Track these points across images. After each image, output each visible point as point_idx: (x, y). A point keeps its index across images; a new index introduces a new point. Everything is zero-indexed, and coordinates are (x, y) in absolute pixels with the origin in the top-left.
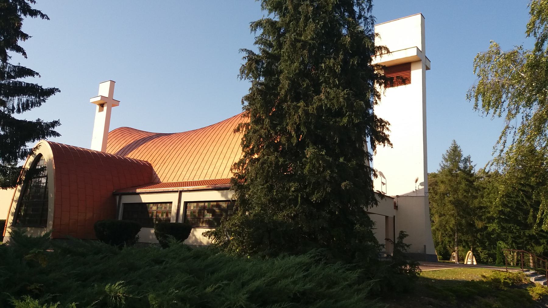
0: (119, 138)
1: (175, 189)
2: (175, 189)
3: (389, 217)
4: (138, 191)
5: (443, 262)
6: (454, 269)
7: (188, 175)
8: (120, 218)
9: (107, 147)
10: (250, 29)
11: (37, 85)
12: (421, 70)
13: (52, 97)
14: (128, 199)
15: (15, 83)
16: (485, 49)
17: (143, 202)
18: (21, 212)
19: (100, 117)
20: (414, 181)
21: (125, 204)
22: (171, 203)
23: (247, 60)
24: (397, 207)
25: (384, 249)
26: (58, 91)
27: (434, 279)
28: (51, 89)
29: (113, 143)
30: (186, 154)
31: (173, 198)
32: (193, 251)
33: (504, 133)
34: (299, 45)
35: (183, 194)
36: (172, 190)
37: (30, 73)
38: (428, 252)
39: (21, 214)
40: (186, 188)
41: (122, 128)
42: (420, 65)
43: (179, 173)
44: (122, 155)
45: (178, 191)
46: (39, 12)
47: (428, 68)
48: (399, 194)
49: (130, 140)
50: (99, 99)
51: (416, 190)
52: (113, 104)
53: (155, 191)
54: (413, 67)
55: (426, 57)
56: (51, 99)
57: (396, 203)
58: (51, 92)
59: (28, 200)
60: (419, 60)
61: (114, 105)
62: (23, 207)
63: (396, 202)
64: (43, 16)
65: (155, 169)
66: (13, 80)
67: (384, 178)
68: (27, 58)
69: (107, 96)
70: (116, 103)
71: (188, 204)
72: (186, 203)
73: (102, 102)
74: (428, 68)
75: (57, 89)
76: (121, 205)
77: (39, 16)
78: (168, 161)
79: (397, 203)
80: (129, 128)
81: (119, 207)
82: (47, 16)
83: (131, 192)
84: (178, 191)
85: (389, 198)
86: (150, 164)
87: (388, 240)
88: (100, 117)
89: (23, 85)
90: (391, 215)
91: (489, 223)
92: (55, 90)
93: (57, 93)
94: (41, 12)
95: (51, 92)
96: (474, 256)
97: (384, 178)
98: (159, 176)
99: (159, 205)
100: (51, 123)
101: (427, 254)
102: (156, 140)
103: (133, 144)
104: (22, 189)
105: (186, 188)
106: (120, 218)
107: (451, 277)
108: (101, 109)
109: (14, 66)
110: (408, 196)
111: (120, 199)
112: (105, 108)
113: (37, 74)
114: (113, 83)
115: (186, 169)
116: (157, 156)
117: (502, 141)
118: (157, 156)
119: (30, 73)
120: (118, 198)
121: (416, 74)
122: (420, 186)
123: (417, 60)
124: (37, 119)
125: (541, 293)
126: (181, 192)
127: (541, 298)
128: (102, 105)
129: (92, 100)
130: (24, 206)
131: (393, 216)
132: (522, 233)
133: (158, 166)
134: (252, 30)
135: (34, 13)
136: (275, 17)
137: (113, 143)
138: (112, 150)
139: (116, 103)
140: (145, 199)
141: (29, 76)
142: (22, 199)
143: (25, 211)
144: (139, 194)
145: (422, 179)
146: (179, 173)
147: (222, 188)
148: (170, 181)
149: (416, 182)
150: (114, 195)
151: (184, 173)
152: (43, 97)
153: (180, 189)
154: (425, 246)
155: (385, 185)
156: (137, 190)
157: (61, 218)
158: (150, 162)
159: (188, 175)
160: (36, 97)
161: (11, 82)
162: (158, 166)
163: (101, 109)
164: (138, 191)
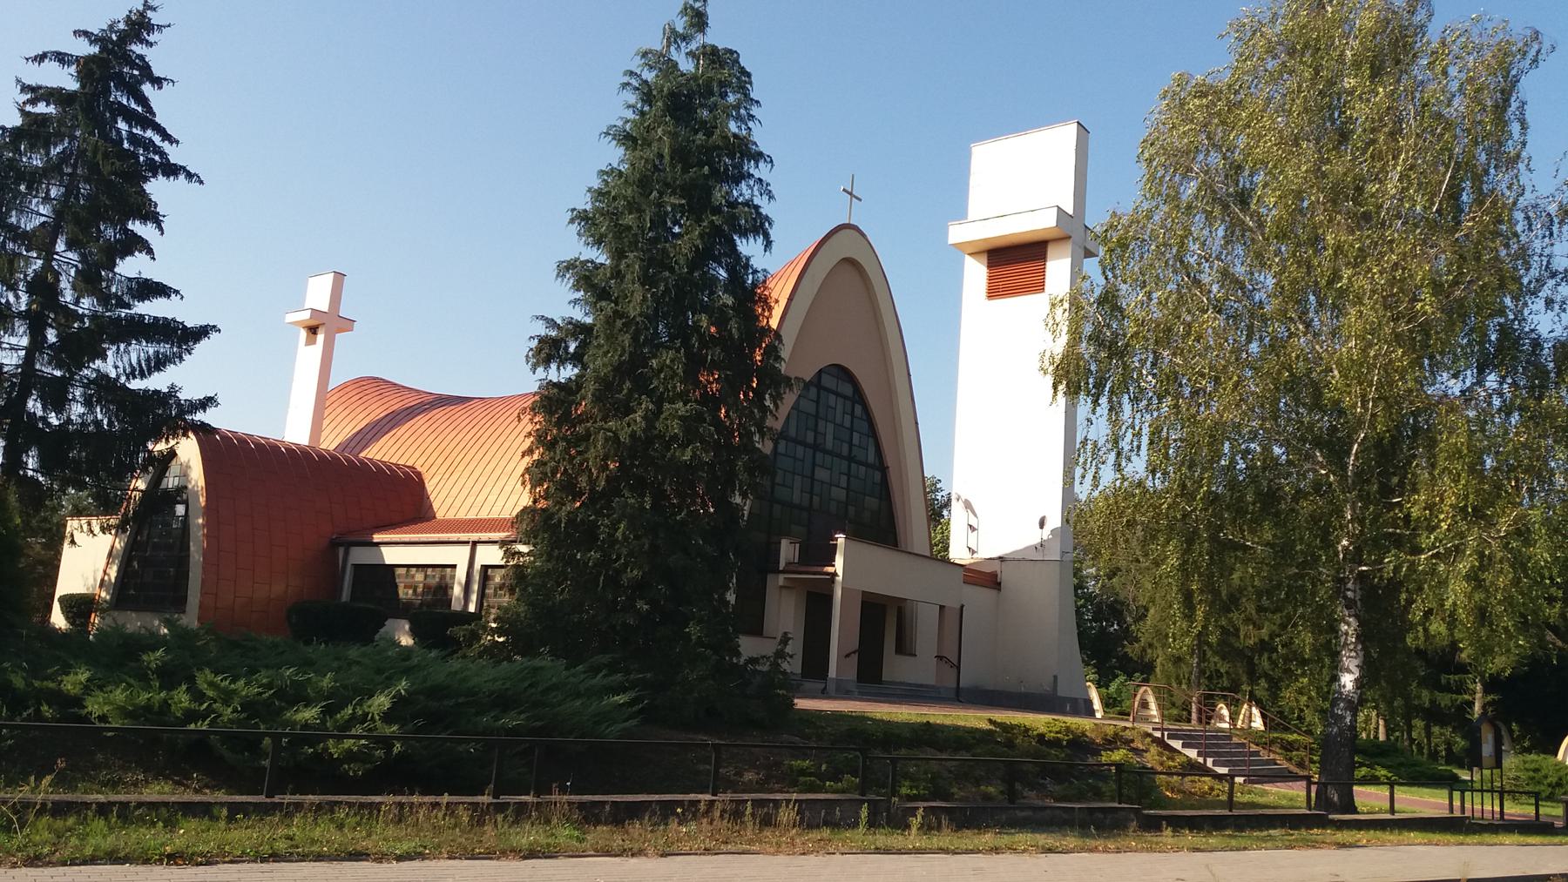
0: (353, 407)
1: (463, 537)
2: (463, 537)
4: (377, 538)
7: (500, 503)
8: (346, 596)
9: (324, 427)
10: (555, 273)
11: (174, 320)
12: (1068, 261)
13: (204, 342)
14: (360, 556)
15: (132, 318)
17: (387, 562)
19: (309, 356)
21: (356, 567)
22: (454, 566)
23: (536, 341)
28: (201, 327)
29: (339, 418)
30: (499, 455)
31: (457, 556)
32: (1132, 829)
34: (619, 323)
35: (480, 548)
36: (455, 539)
37: (162, 290)
40: (485, 536)
42: (1068, 248)
43: (481, 498)
45: (468, 542)
46: (184, 168)
49: (377, 411)
50: (306, 315)
53: (422, 540)
54: (1051, 251)
56: (202, 347)
58: (202, 332)
63: (999, 573)
65: (429, 487)
66: (127, 311)
67: (975, 515)
68: (154, 259)
69: (326, 310)
70: (347, 324)
71: (490, 570)
72: (485, 568)
75: (214, 327)
76: (349, 569)
77: (182, 177)
78: (461, 468)
80: (378, 378)
84: (468, 542)
86: (419, 474)
88: (309, 356)
89: (146, 321)
90: (952, 603)
93: (214, 335)
94: (188, 168)
95: (202, 332)
97: (975, 515)
98: (435, 506)
99: (430, 570)
100: (200, 400)
102: (437, 413)
103: (385, 421)
105: (485, 536)
106: (346, 596)
108: (311, 341)
109: (130, 279)
110: (1024, 560)
111: (347, 554)
112: (320, 337)
113: (177, 292)
114: (339, 277)
115: (496, 490)
116: (435, 454)
118: (435, 454)
119: (162, 290)
120: (341, 551)
124: (169, 384)
126: (475, 544)
128: (313, 330)
129: (292, 317)
133: (435, 480)
134: (558, 276)
135: (172, 170)
136: (601, 257)
137: (339, 418)
138: (330, 442)
139: (347, 324)
140: (391, 556)
141: (160, 296)
144: (378, 544)
145: (1055, 521)
146: (481, 498)
148: (461, 515)
150: (334, 544)
151: (492, 498)
152: (186, 343)
153: (474, 536)
154: (1055, 677)
156: (374, 536)
157: (216, 594)
158: (419, 469)
159: (500, 503)
160: (172, 345)
161: (123, 315)
162: (435, 480)
163: (311, 341)
164: (377, 538)
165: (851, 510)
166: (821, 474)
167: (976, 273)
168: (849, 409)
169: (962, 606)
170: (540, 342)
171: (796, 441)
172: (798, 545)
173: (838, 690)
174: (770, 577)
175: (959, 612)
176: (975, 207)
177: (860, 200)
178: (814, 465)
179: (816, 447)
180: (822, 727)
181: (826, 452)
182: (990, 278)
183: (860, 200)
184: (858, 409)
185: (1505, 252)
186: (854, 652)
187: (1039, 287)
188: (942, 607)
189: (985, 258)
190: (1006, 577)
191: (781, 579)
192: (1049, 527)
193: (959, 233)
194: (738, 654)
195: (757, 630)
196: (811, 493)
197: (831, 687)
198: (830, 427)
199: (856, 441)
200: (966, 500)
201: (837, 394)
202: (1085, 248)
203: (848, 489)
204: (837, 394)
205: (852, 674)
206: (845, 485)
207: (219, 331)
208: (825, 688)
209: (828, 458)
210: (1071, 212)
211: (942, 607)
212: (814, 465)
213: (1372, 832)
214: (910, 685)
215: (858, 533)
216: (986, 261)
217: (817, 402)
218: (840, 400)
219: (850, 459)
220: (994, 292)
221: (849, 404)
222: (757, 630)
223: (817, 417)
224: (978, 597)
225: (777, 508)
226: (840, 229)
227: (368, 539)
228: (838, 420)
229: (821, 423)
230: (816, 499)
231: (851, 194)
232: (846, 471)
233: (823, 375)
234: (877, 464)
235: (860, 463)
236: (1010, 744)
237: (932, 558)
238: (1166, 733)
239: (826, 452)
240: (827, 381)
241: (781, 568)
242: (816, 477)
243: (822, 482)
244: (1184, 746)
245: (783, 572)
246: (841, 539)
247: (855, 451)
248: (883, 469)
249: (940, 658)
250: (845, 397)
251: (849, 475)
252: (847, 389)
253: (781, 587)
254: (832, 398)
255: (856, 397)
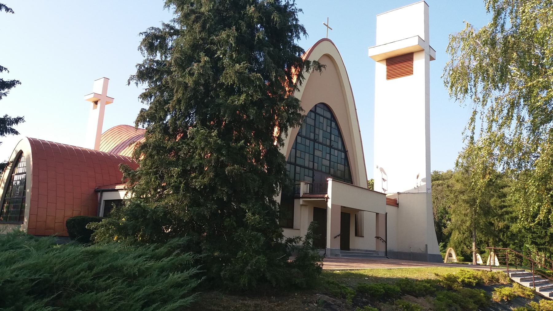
3: (379, 214)
4: (117, 187)
5: (463, 263)
6: (426, 269)
12: (424, 60)
13: (13, 89)
14: (108, 196)
16: (460, 28)
18: (3, 209)
20: (416, 177)
24: (398, 204)
25: (301, 241)
26: (19, 84)
27: (368, 277)
33: (473, 120)
34: (193, 17)
38: (430, 252)
39: (4, 211)
41: (121, 126)
44: (115, 153)
46: (4, 6)
47: (433, 58)
48: (400, 191)
51: (417, 186)
52: (106, 102)
55: (430, 46)
57: (397, 200)
59: (10, 197)
60: (422, 49)
61: (107, 103)
62: (5, 204)
63: (397, 199)
64: (7, 9)
70: (110, 100)
73: (96, 100)
74: (432, 59)
75: (18, 81)
79: (398, 201)
81: (100, 204)
82: (11, 10)
83: (110, 188)
85: (380, 194)
87: (378, 238)
90: (382, 212)
91: (513, 222)
92: (16, 82)
93: (17, 86)
94: (6, 6)
95: (11, 84)
96: (496, 256)
100: (15, 119)
101: (429, 254)
104: (5, 186)
107: (388, 275)
108: (95, 108)
110: (409, 193)
111: (101, 195)
113: (6, 69)
114: (107, 79)
117: (472, 127)
120: (99, 194)
121: (419, 63)
122: (422, 182)
123: (417, 51)
125: (508, 294)
127: (509, 299)
128: (96, 103)
130: (6, 203)
131: (385, 214)
132: (544, 232)
138: (106, 148)
139: (110, 100)
142: (5, 196)
143: (8, 208)
144: (117, 190)
145: (423, 175)
147: (18, 163)
149: (417, 178)
150: (96, 192)
154: (426, 245)
155: (386, 182)
156: (116, 186)
163: (95, 108)
165: (332, 170)
166: (317, 153)
167: (382, 68)
168: (329, 124)
169: (386, 214)
170: (146, 36)
171: (306, 138)
172: (308, 185)
173: (331, 254)
174: (296, 201)
175: (385, 216)
176: (380, 38)
177: (331, 29)
178: (314, 149)
179: (315, 141)
180: (344, 288)
181: (319, 143)
182: (388, 71)
183: (331, 29)
184: (333, 124)
185: (533, 101)
186: (338, 236)
187: (410, 72)
188: (377, 214)
189: (385, 62)
190: (401, 201)
191: (301, 201)
192: (421, 178)
193: (372, 52)
194: (281, 236)
195: (290, 226)
196: (313, 162)
197: (328, 253)
198: (321, 132)
199: (333, 139)
200: (381, 168)
201: (324, 117)
202: (430, 56)
203: (330, 160)
204: (324, 117)
205: (338, 246)
206: (329, 159)
207: (21, 83)
208: (325, 253)
209: (321, 146)
210: (424, 40)
211: (377, 214)
212: (314, 149)
213: (429, 278)
214: (361, 250)
215: (336, 178)
216: (385, 64)
217: (315, 120)
218: (325, 120)
219: (331, 147)
220: (390, 76)
221: (329, 121)
222: (290, 226)
223: (315, 126)
224: (391, 210)
225: (298, 168)
226: (323, 41)
227: (113, 188)
228: (325, 129)
229: (317, 130)
230: (316, 165)
231: (327, 26)
232: (329, 152)
233: (317, 108)
234: (343, 150)
235: (335, 149)
236: (450, 288)
237: (368, 190)
238: (510, 274)
239: (319, 143)
240: (319, 110)
241: (301, 196)
242: (315, 155)
243: (318, 157)
244: (522, 280)
245: (302, 198)
246: (330, 182)
247: (333, 143)
248: (345, 152)
249: (377, 237)
250: (327, 119)
251: (330, 154)
252: (328, 115)
253: (302, 205)
254: (322, 118)
255: (332, 119)
